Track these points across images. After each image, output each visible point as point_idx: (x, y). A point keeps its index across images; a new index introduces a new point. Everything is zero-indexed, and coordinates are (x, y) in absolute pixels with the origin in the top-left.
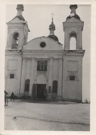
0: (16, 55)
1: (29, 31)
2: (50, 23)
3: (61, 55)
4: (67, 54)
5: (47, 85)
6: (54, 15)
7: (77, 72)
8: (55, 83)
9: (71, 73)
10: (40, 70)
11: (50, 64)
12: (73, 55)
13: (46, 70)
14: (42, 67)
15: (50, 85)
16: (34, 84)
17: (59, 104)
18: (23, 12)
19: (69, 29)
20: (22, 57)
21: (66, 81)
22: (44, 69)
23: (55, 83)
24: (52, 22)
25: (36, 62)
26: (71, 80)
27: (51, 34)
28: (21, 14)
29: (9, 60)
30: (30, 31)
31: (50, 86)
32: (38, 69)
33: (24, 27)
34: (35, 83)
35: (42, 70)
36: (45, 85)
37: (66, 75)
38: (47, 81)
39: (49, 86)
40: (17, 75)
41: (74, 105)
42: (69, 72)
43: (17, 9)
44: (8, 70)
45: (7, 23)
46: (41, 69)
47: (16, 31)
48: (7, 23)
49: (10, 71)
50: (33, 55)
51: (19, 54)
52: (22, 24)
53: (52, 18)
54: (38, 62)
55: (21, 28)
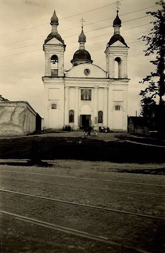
3: (106, 84)
4: (113, 83)
6: (85, 21)
7: (123, 102)
8: (100, 114)
9: (116, 103)
10: (84, 100)
11: (94, 93)
12: (119, 84)
13: (90, 99)
14: (86, 97)
15: (96, 116)
17: (3, 139)
19: (114, 54)
21: (112, 111)
22: (88, 98)
23: (100, 114)
24: (82, 31)
25: (80, 91)
26: (91, 100)
28: (56, 30)
31: (96, 117)
32: (82, 99)
35: (86, 100)
36: (90, 116)
37: (112, 105)
39: (95, 117)
40: (60, 104)
42: (114, 102)
46: (84, 98)
47: (56, 54)
49: (51, 101)
50: (77, 83)
52: (62, 47)
53: (82, 25)
54: (82, 90)
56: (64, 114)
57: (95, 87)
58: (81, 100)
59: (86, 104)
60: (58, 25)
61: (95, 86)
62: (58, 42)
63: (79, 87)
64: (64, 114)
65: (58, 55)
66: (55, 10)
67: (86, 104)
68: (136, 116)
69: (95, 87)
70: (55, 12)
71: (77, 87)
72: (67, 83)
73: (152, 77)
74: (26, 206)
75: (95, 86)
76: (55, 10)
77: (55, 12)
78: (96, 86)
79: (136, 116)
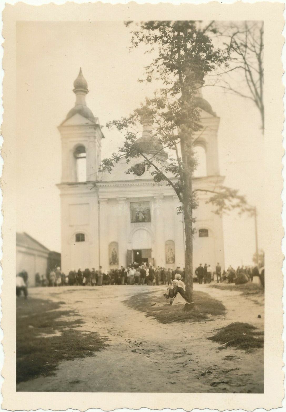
0: (84, 193)
1: (103, 137)
2: (254, 251)
5: (153, 249)
16: (128, 250)
18: (87, 95)
20: (98, 196)
27: (138, 144)
29: (70, 205)
30: (105, 136)
33: (95, 133)
34: (130, 249)
38: (154, 242)
41: (183, 250)
43: (75, 91)
44: (71, 226)
45: (57, 185)
48: (57, 185)
51: (91, 191)
52: (91, 128)
55: (89, 137)
56: (99, 247)
57: (157, 195)
58: (131, 222)
59: (140, 229)
60: (87, 93)
61: (155, 194)
62: (84, 121)
63: (125, 198)
64: (99, 247)
65: (85, 144)
66: (81, 68)
67: (140, 229)
68: (149, 159)
69: (155, 196)
70: (81, 71)
71: (122, 198)
72: (102, 192)
73: (233, 46)
74: (173, 381)
75: (155, 195)
76: (81, 68)
77: (81, 71)
78: (158, 194)
79: (149, 159)
